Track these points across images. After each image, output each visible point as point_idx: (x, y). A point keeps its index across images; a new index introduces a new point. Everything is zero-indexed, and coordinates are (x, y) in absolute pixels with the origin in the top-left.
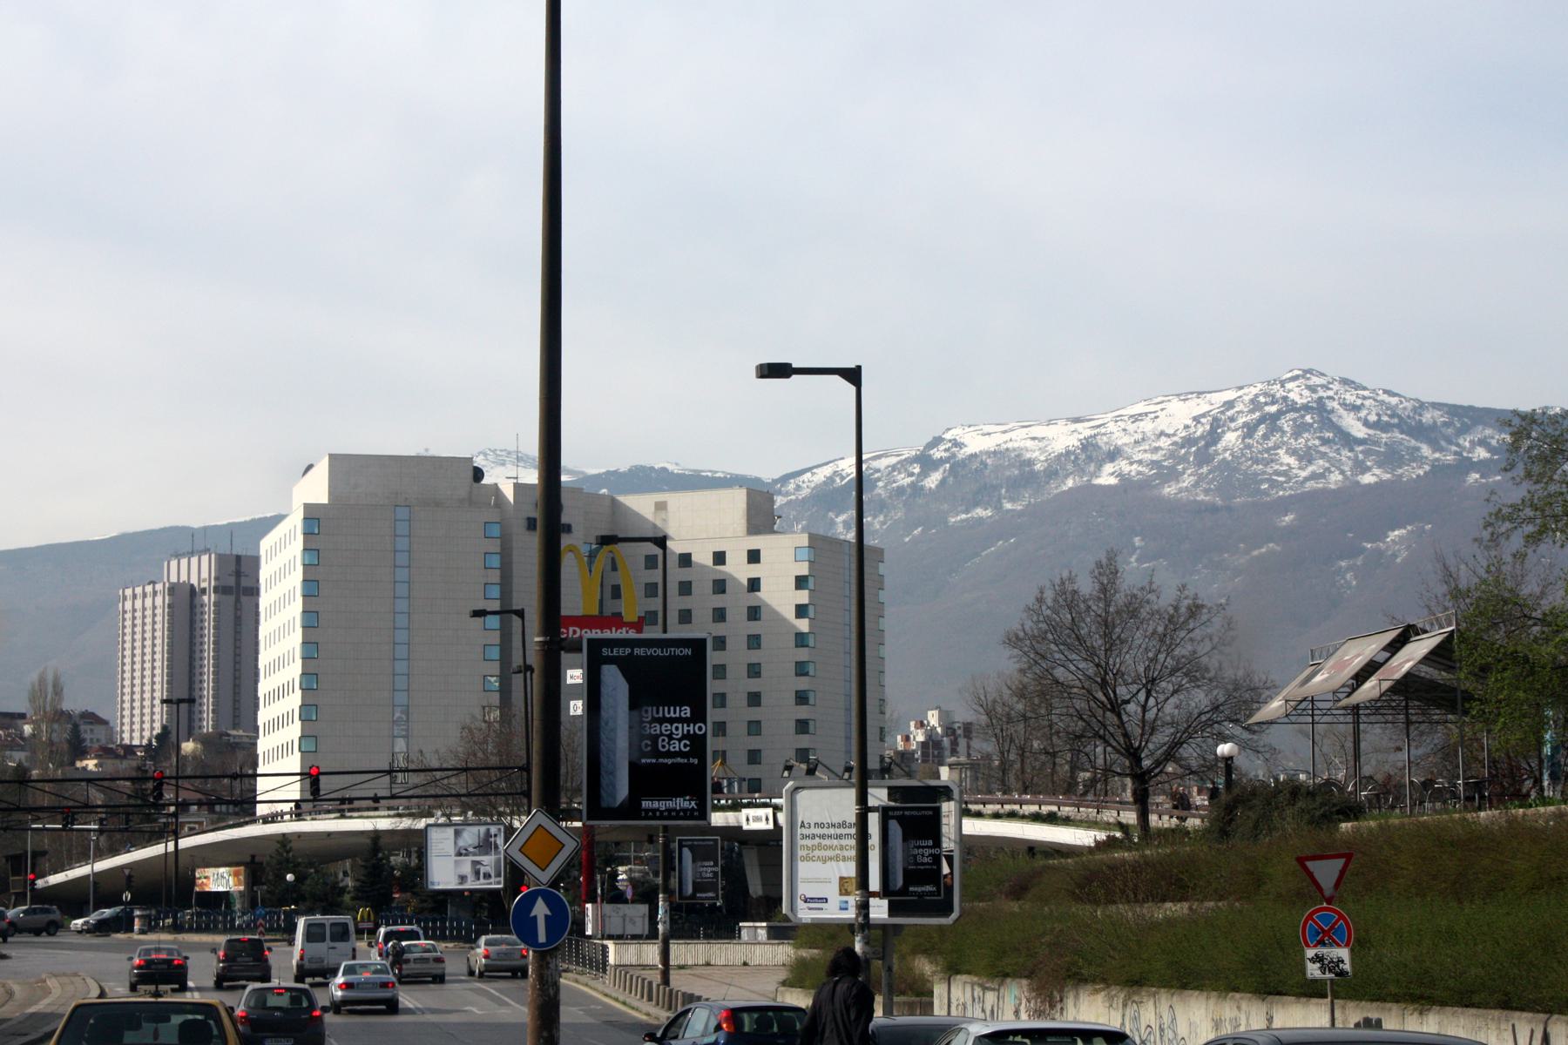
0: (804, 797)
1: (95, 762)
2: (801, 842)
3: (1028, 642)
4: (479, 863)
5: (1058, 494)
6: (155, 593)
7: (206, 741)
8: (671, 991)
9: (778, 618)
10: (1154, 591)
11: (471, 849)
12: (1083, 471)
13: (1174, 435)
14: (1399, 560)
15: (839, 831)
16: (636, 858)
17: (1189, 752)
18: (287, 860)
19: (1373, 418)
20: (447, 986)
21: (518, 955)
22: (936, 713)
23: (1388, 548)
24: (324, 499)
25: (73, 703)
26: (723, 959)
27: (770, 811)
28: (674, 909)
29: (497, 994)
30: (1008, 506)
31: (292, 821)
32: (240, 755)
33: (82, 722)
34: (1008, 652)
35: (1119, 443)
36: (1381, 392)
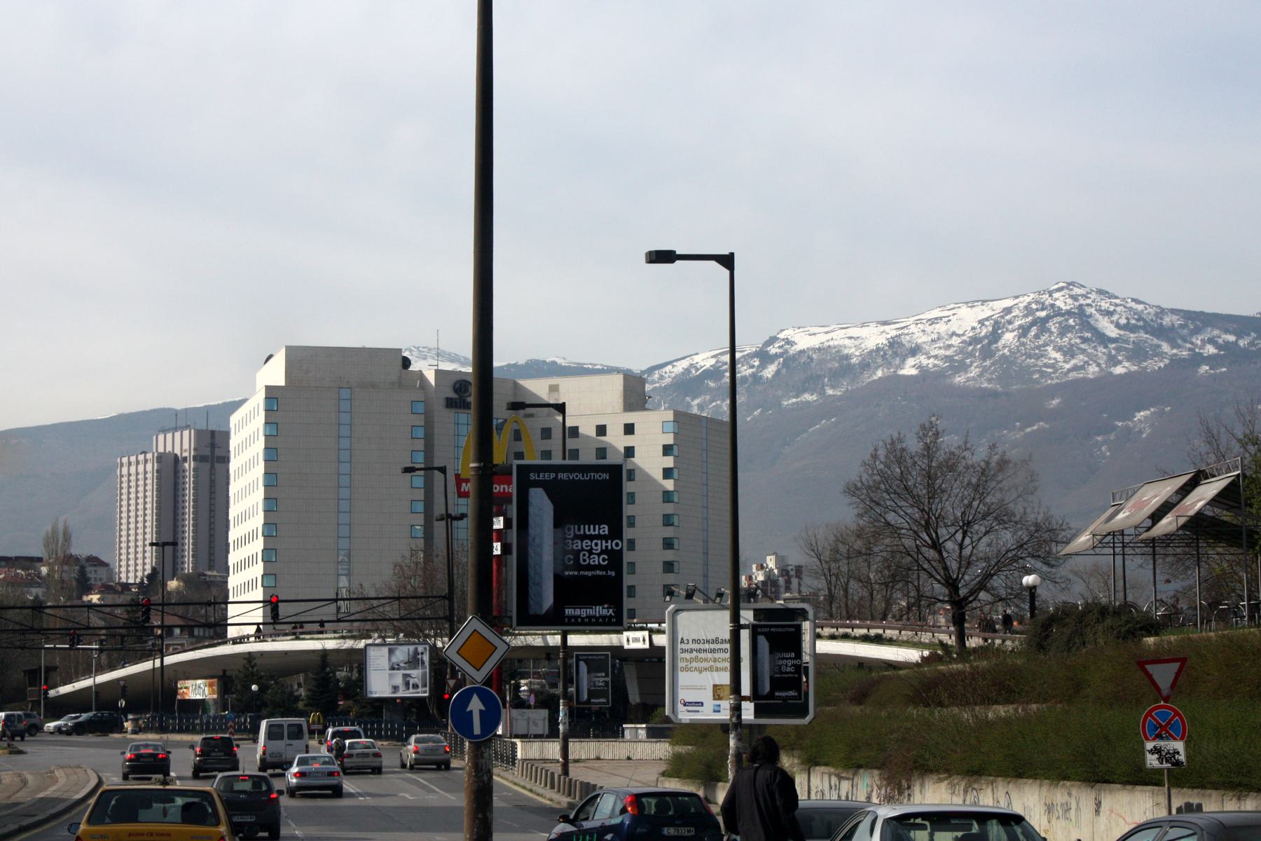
0: (683, 618)
1: (98, 596)
2: (681, 656)
3: (865, 491)
4: (409, 675)
5: (871, 382)
6: (146, 461)
7: (187, 580)
8: (570, 780)
9: (649, 479)
10: (968, 449)
11: (402, 665)
12: (890, 363)
13: (963, 335)
14: (1144, 436)
15: (712, 646)
16: (534, 673)
17: (997, 582)
18: (252, 674)
19: (1123, 321)
20: (383, 776)
21: (441, 751)
22: (773, 557)
23: (1135, 426)
24: (282, 382)
25: (80, 549)
26: (610, 754)
27: (646, 633)
28: (571, 713)
29: (425, 783)
30: (830, 392)
31: (256, 642)
32: (214, 591)
33: (87, 565)
34: (848, 499)
35: (919, 341)
36: (1130, 300)
